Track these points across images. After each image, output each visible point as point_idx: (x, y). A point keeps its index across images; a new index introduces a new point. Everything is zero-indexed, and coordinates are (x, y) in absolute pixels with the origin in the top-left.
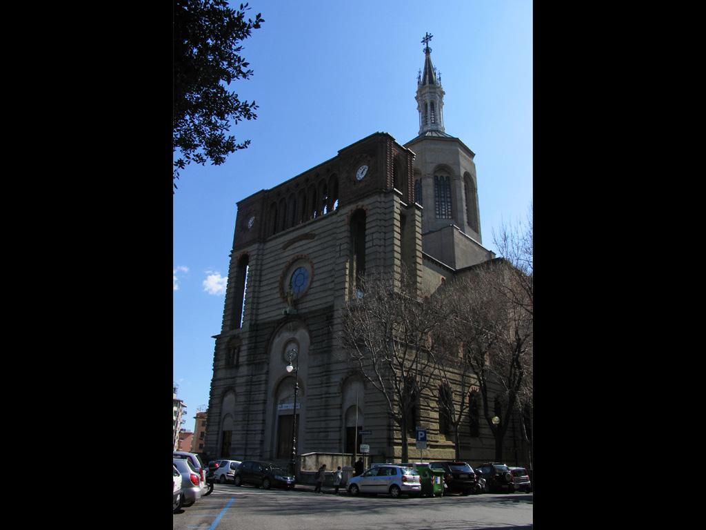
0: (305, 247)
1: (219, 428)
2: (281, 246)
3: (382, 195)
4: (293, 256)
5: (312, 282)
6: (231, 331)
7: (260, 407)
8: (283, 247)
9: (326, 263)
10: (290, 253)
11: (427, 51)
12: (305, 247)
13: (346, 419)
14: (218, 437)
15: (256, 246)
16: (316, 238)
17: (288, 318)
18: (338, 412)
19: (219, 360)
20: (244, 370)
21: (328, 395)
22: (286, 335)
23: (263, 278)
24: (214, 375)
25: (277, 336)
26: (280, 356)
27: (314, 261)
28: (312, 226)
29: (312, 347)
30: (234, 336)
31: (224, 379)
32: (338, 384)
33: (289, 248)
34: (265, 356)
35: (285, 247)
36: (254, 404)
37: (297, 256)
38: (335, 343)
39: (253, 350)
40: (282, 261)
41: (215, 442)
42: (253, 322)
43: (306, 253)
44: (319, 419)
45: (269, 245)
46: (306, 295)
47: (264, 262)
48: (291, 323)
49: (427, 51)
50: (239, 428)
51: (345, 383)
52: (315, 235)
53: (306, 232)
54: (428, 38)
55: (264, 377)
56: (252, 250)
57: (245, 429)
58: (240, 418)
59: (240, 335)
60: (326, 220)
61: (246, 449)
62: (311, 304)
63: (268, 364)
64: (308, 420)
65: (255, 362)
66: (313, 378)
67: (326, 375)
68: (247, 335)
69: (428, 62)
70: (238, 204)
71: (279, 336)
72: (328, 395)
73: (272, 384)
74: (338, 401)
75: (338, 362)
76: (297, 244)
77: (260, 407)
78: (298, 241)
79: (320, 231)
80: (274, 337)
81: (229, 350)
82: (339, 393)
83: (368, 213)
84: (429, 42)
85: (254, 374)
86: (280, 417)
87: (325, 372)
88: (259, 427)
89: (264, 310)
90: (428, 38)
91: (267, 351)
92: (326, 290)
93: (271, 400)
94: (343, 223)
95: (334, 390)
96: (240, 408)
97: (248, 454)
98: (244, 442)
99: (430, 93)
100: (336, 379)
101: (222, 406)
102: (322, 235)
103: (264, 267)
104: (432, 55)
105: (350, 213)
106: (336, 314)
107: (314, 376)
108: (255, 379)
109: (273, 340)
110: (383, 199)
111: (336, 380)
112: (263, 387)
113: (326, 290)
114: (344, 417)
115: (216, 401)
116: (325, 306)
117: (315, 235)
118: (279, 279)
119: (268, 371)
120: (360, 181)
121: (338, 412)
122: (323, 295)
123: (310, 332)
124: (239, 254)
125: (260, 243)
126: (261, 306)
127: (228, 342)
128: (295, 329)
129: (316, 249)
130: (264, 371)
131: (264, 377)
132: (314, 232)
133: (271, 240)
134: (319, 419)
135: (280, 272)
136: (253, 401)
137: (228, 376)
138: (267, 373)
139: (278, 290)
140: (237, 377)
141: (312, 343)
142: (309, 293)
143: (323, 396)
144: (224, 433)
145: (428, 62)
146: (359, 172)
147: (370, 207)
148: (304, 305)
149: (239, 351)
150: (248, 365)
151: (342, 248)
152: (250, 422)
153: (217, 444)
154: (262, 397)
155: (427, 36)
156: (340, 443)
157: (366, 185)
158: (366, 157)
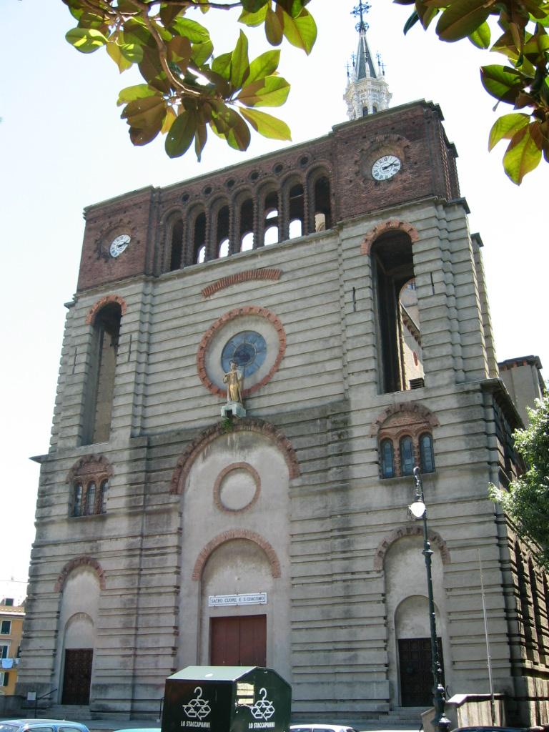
0: (257, 294)
1: (56, 643)
2: (198, 290)
3: (441, 207)
4: (228, 310)
5: (281, 357)
6: (83, 448)
7: (169, 601)
8: (207, 290)
9: (314, 324)
10: (221, 303)
11: (362, 27)
12: (257, 294)
13: (397, 623)
14: (55, 663)
15: (139, 287)
16: (284, 278)
17: (230, 423)
18: (379, 610)
19: (51, 505)
20: (120, 526)
21: (349, 577)
22: (220, 458)
23: (155, 348)
24: (39, 535)
25: (201, 457)
26: (211, 498)
27: (283, 320)
28: (272, 256)
29: (296, 482)
30: (92, 456)
31: (66, 543)
32: (374, 552)
33: (217, 295)
34: (174, 498)
35: (208, 292)
36: (149, 594)
37: (230, 314)
38: (357, 472)
39: (143, 485)
40: (200, 318)
41: (49, 673)
42: (138, 431)
43: (262, 304)
44: (330, 624)
45: (163, 288)
46: (267, 381)
47: (157, 319)
48: (234, 436)
49: (362, 27)
50: (116, 642)
51: (388, 553)
52: (282, 273)
53: (258, 266)
54: (361, 9)
55: (172, 540)
56: (130, 295)
57: (132, 645)
58: (116, 622)
59: (107, 456)
60: (306, 247)
61: (133, 686)
62: (275, 400)
63: (181, 514)
64: (295, 626)
65: (149, 508)
66: (326, 539)
67: (343, 537)
68: (126, 455)
69: (363, 42)
70: (85, 209)
71: (204, 458)
72: (349, 577)
73: (193, 554)
74: (379, 587)
75: (368, 511)
76: (236, 288)
77: (169, 601)
78: (222, 288)
79: (295, 265)
80: (193, 462)
81: (77, 485)
82: (379, 572)
83: (415, 237)
84: (364, 15)
85: (145, 534)
86: (214, 621)
87: (339, 530)
88: (167, 641)
89: (161, 410)
90: (361, 9)
91: (177, 487)
92: (320, 374)
93: (189, 585)
94: (357, 252)
95: (366, 564)
96: (116, 603)
97: (138, 697)
98: (129, 673)
99: (373, 90)
100: (372, 543)
101: (61, 597)
102: (300, 274)
103: (156, 328)
104: (369, 35)
105: (90, 316)
106: (355, 419)
107: (307, 538)
108: (150, 543)
109: (191, 466)
110: (443, 214)
111: (370, 545)
112: (172, 560)
113: (320, 374)
114: (391, 617)
115: (46, 588)
116: (318, 403)
117: (282, 273)
118: (196, 350)
119: (180, 529)
120: (377, 183)
121: (379, 610)
122: (308, 382)
123: (290, 453)
124: (93, 301)
125: (146, 282)
126: (151, 401)
127: (75, 470)
128: (246, 446)
129: (285, 298)
130: (174, 528)
131: (172, 540)
132: (276, 268)
133: (167, 280)
134: (330, 624)
135: (199, 338)
136: (147, 588)
137: (78, 537)
138: (180, 531)
139: (194, 371)
140: (101, 539)
141: (295, 474)
142: (275, 378)
143: (338, 577)
144: (69, 654)
145: (363, 42)
146: (116, 243)
147: (419, 226)
148: (264, 402)
149: (102, 489)
150: (131, 515)
151: (76, 371)
152: (141, 631)
153: (53, 675)
154: (171, 580)
155: (361, 4)
156: (387, 672)
157: (405, 189)
158: (399, 139)
